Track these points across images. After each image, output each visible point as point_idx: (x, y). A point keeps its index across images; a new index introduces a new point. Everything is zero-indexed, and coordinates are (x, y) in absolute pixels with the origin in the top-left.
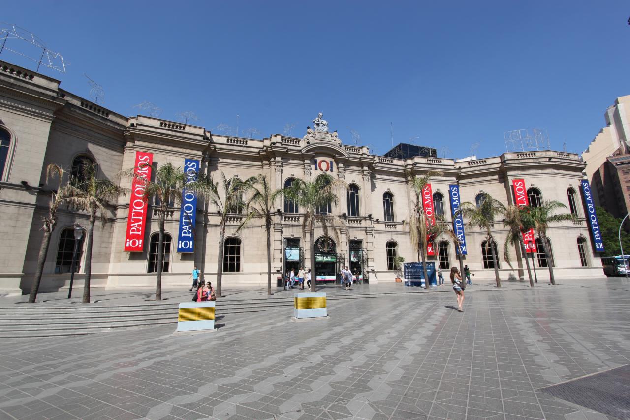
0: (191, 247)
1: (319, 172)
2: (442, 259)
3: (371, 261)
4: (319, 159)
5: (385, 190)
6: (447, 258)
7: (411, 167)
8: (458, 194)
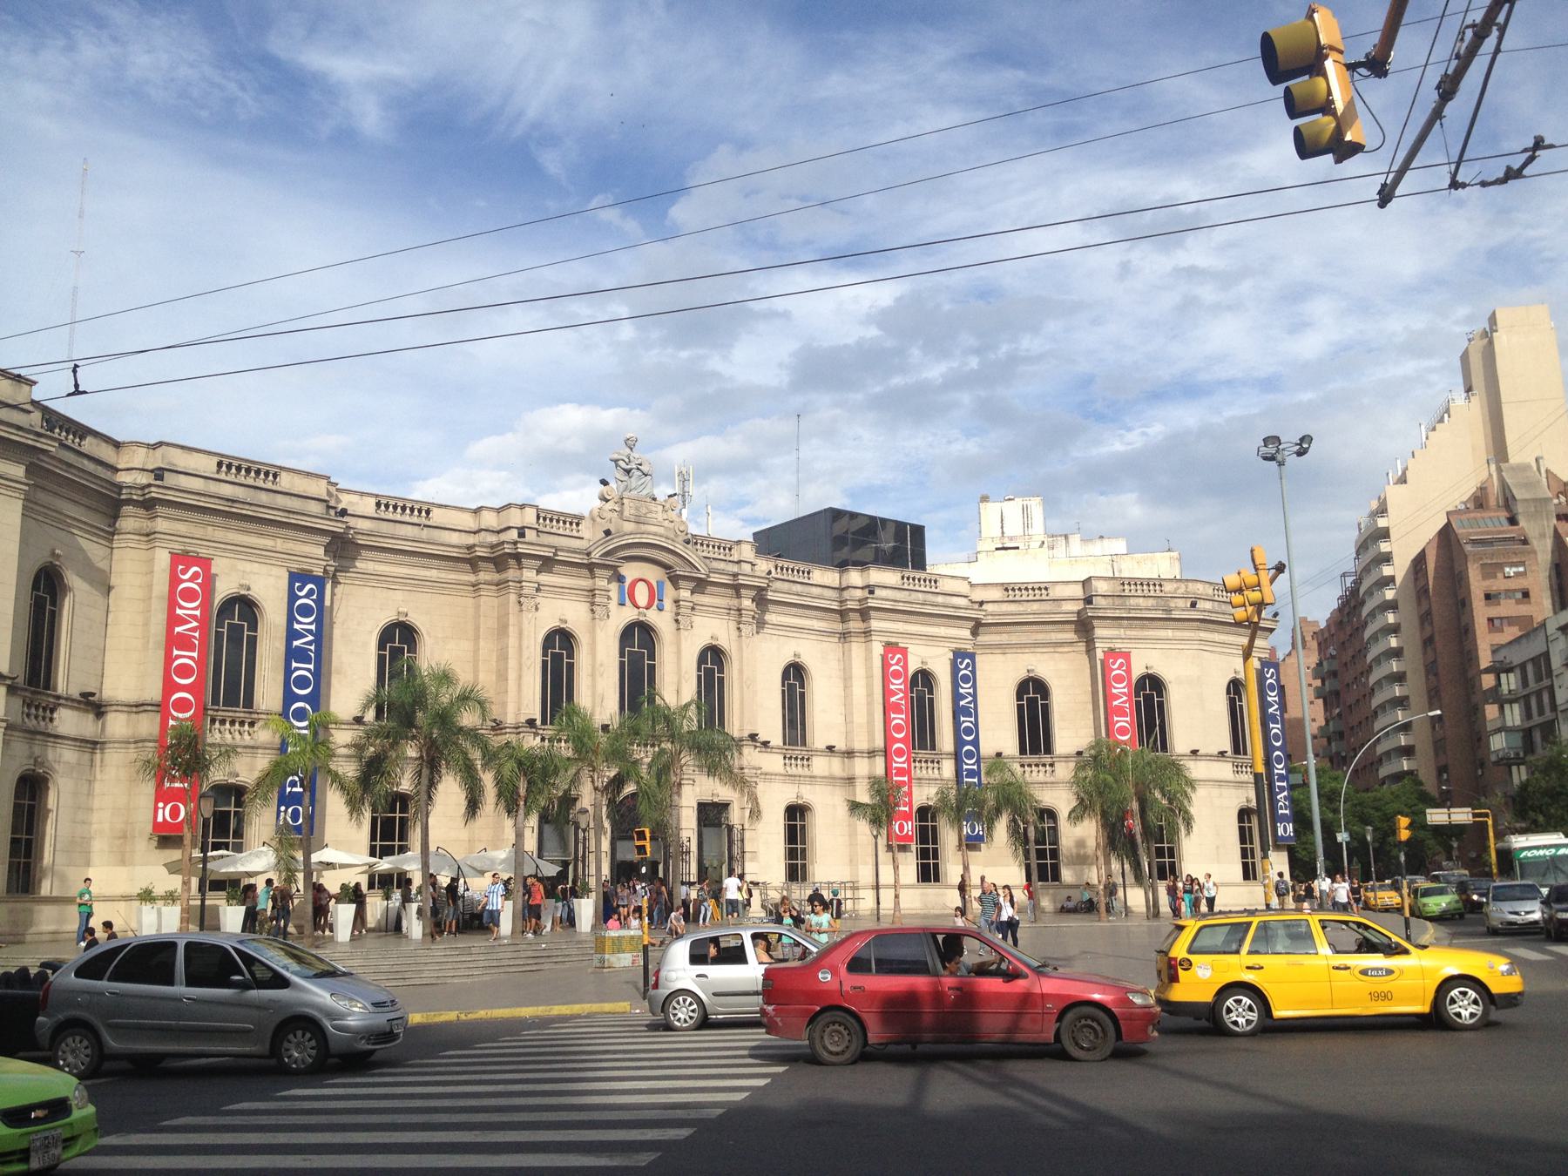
1: (629, 614)
2: (923, 854)
3: (752, 860)
4: (631, 571)
6: (936, 851)
8: (971, 679)
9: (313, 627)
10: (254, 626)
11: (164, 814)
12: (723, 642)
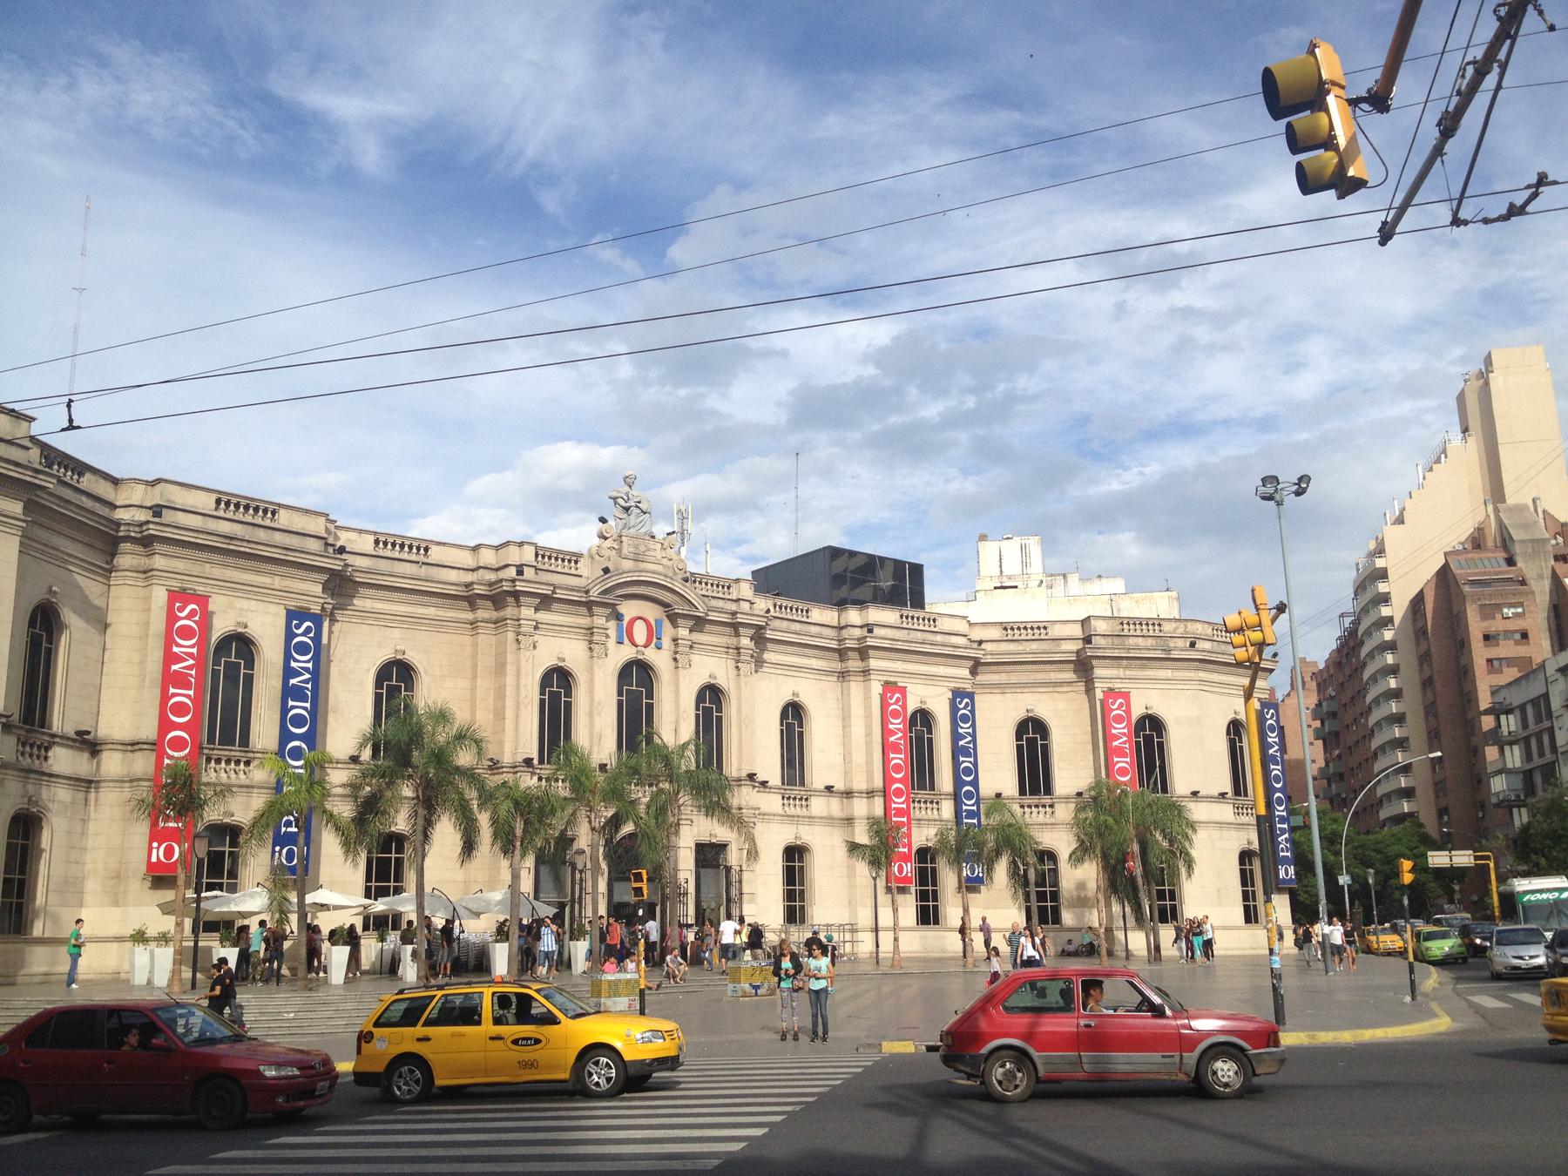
1: (627, 653)
2: (923, 896)
4: (629, 609)
5: (788, 697)
6: (935, 893)
7: (857, 632)
8: (971, 718)
10: (250, 664)
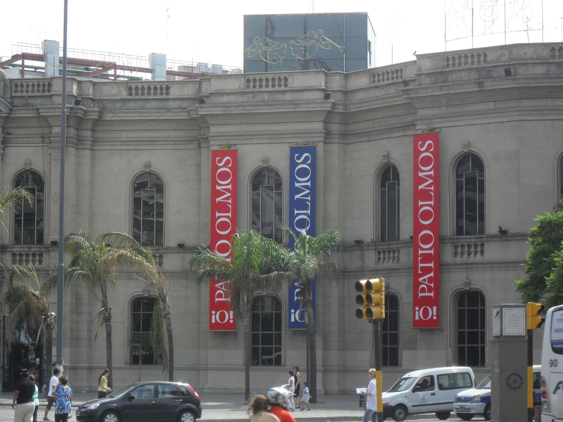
0: (231, 321)
9: (230, 187)
11: (216, 318)
12: (38, 166)
